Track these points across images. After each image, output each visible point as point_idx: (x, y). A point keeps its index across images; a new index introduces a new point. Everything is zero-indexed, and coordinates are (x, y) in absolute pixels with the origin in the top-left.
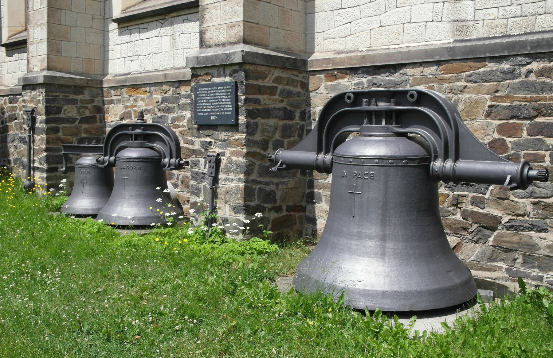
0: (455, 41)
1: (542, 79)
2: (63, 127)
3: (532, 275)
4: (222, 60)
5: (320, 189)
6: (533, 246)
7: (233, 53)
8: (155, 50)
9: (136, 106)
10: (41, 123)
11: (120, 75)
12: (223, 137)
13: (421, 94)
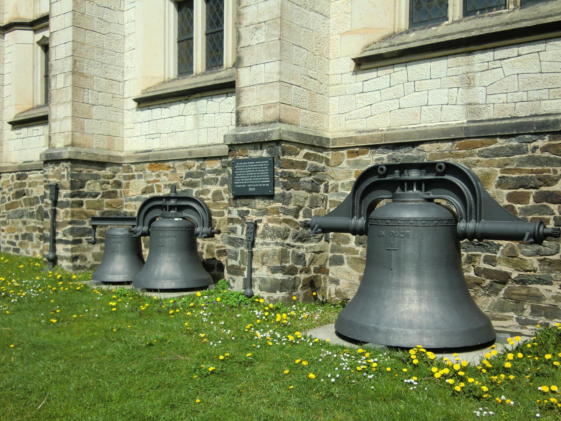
0: (468, 122)
1: (546, 154)
2: (87, 201)
3: (540, 322)
4: (260, 137)
5: (343, 253)
6: (539, 298)
7: (271, 131)
8: (178, 129)
9: (158, 181)
10: (65, 196)
11: (141, 152)
12: (260, 206)
13: (448, 165)
